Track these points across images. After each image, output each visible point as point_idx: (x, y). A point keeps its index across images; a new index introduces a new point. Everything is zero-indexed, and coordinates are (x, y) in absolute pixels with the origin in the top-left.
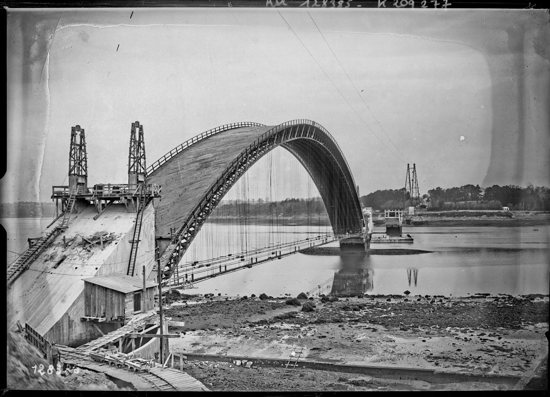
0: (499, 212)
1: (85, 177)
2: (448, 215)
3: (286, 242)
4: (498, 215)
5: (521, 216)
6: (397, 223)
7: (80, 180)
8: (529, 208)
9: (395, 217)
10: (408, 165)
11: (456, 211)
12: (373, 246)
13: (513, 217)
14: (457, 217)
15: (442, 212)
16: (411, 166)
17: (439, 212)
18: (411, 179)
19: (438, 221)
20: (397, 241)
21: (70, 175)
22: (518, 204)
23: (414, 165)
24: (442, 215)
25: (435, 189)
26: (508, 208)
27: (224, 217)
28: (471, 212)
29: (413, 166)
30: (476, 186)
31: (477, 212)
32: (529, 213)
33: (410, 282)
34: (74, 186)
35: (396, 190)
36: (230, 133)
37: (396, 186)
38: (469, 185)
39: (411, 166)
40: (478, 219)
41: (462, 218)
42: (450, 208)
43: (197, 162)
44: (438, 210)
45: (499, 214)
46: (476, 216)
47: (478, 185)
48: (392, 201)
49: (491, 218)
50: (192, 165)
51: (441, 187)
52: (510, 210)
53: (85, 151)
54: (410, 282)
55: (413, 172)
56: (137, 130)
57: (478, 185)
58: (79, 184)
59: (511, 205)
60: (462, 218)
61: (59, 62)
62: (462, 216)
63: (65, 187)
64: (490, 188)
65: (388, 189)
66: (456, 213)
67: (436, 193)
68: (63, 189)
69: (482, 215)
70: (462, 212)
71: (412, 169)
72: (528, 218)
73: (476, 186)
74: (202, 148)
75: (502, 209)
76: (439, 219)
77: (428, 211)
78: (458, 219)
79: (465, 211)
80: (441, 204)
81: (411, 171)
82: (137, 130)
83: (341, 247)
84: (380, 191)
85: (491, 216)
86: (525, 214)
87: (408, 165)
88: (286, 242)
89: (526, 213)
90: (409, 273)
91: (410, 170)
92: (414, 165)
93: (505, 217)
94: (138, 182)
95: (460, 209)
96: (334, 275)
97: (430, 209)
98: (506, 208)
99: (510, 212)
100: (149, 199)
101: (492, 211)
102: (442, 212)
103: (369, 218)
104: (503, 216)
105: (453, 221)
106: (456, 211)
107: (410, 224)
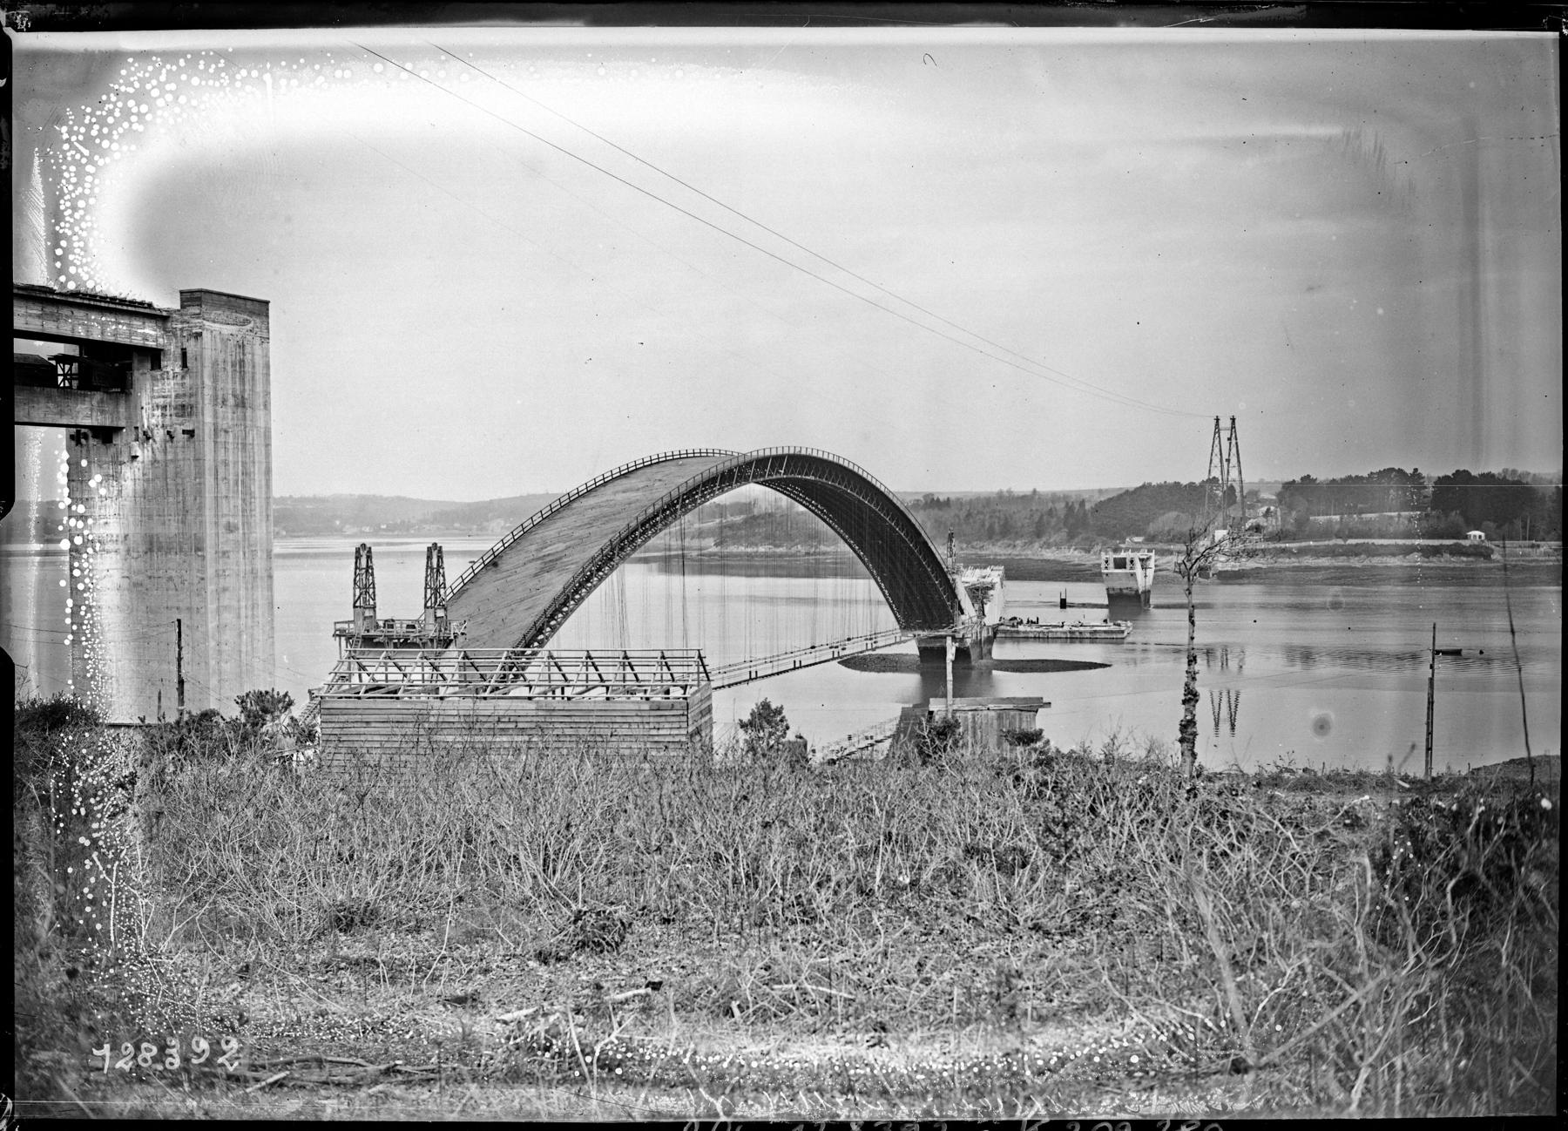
0: (1455, 545)
1: (374, 608)
2: (1316, 553)
3: (814, 638)
4: (1452, 554)
5: (1517, 555)
6: (1131, 584)
7: (368, 613)
8: (1542, 533)
9: (1127, 571)
10: (1217, 420)
11: (1340, 542)
12: (1000, 652)
13: (1494, 557)
14: (1342, 558)
15: (1304, 544)
16: (1225, 423)
17: (1294, 545)
18: (1225, 456)
19: (1288, 569)
20: (1088, 635)
21: (355, 607)
22: (1512, 523)
23: (1233, 420)
24: (1302, 552)
25: (1298, 479)
26: (1483, 534)
27: (749, 550)
28: (1382, 545)
29: (1229, 422)
30: (1409, 471)
31: (1397, 546)
32: (1538, 546)
33: (1217, 725)
34: (360, 622)
35: (1191, 484)
36: (607, 494)
37: (1195, 474)
38: (1392, 470)
39: (1225, 423)
40: (1399, 563)
41: (1355, 562)
42: (1326, 533)
43: (539, 559)
44: (1294, 540)
45: (1457, 551)
46: (1394, 555)
47: (1416, 470)
48: (1173, 514)
49: (1435, 559)
50: (529, 565)
51: (1313, 476)
52: (1488, 538)
53: (372, 575)
54: (1217, 725)
55: (1229, 439)
56: (435, 554)
57: (1416, 470)
58: (365, 618)
59: (1492, 525)
60: (1355, 562)
61: (317, 67)
62: (1356, 555)
63: (349, 622)
64: (1447, 477)
65: (1171, 481)
66: (1341, 546)
67: (1297, 491)
68: (346, 626)
69: (1409, 554)
70: (1357, 545)
71: (1226, 431)
72: (1537, 561)
73: (1409, 471)
74: (550, 531)
75: (1466, 537)
76: (1293, 562)
77: (1267, 540)
78: (1346, 564)
79: (1366, 541)
80: (1301, 523)
81: (1225, 435)
82: (435, 554)
83: (921, 656)
84: (1150, 484)
85: (1434, 555)
86: (1527, 550)
87: (1217, 420)
88: (814, 638)
89: (1533, 546)
90: (1216, 701)
91: (1222, 433)
92: (1233, 420)
93: (1471, 559)
94: (436, 618)
95: (1351, 537)
96: (899, 714)
97: (1279, 536)
98: (1477, 533)
99: (1488, 544)
100: (447, 643)
101: (1436, 542)
102: (1304, 544)
103: (991, 592)
104: (1467, 555)
105: (1327, 568)
106: (1340, 542)
107: (1208, 578)
